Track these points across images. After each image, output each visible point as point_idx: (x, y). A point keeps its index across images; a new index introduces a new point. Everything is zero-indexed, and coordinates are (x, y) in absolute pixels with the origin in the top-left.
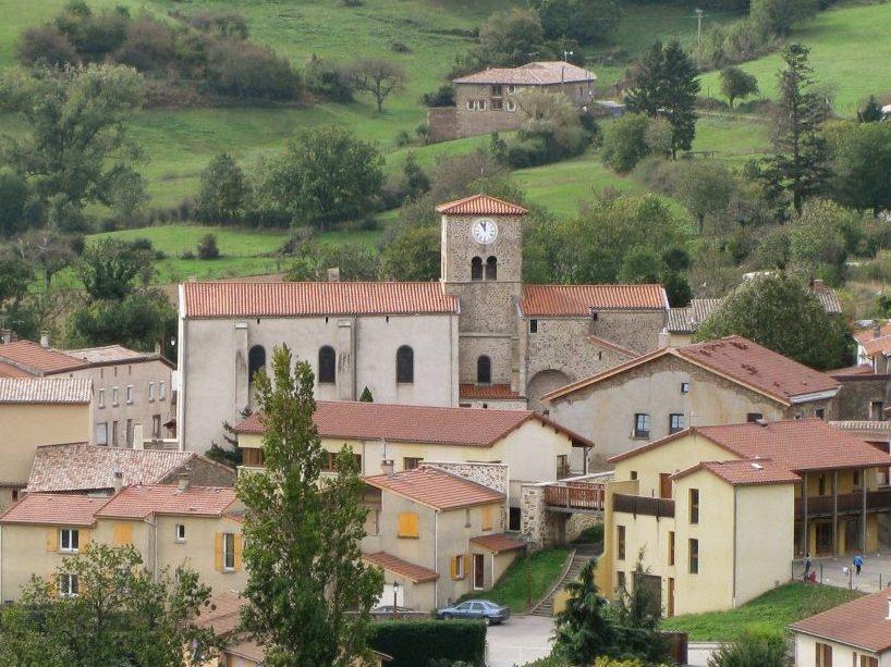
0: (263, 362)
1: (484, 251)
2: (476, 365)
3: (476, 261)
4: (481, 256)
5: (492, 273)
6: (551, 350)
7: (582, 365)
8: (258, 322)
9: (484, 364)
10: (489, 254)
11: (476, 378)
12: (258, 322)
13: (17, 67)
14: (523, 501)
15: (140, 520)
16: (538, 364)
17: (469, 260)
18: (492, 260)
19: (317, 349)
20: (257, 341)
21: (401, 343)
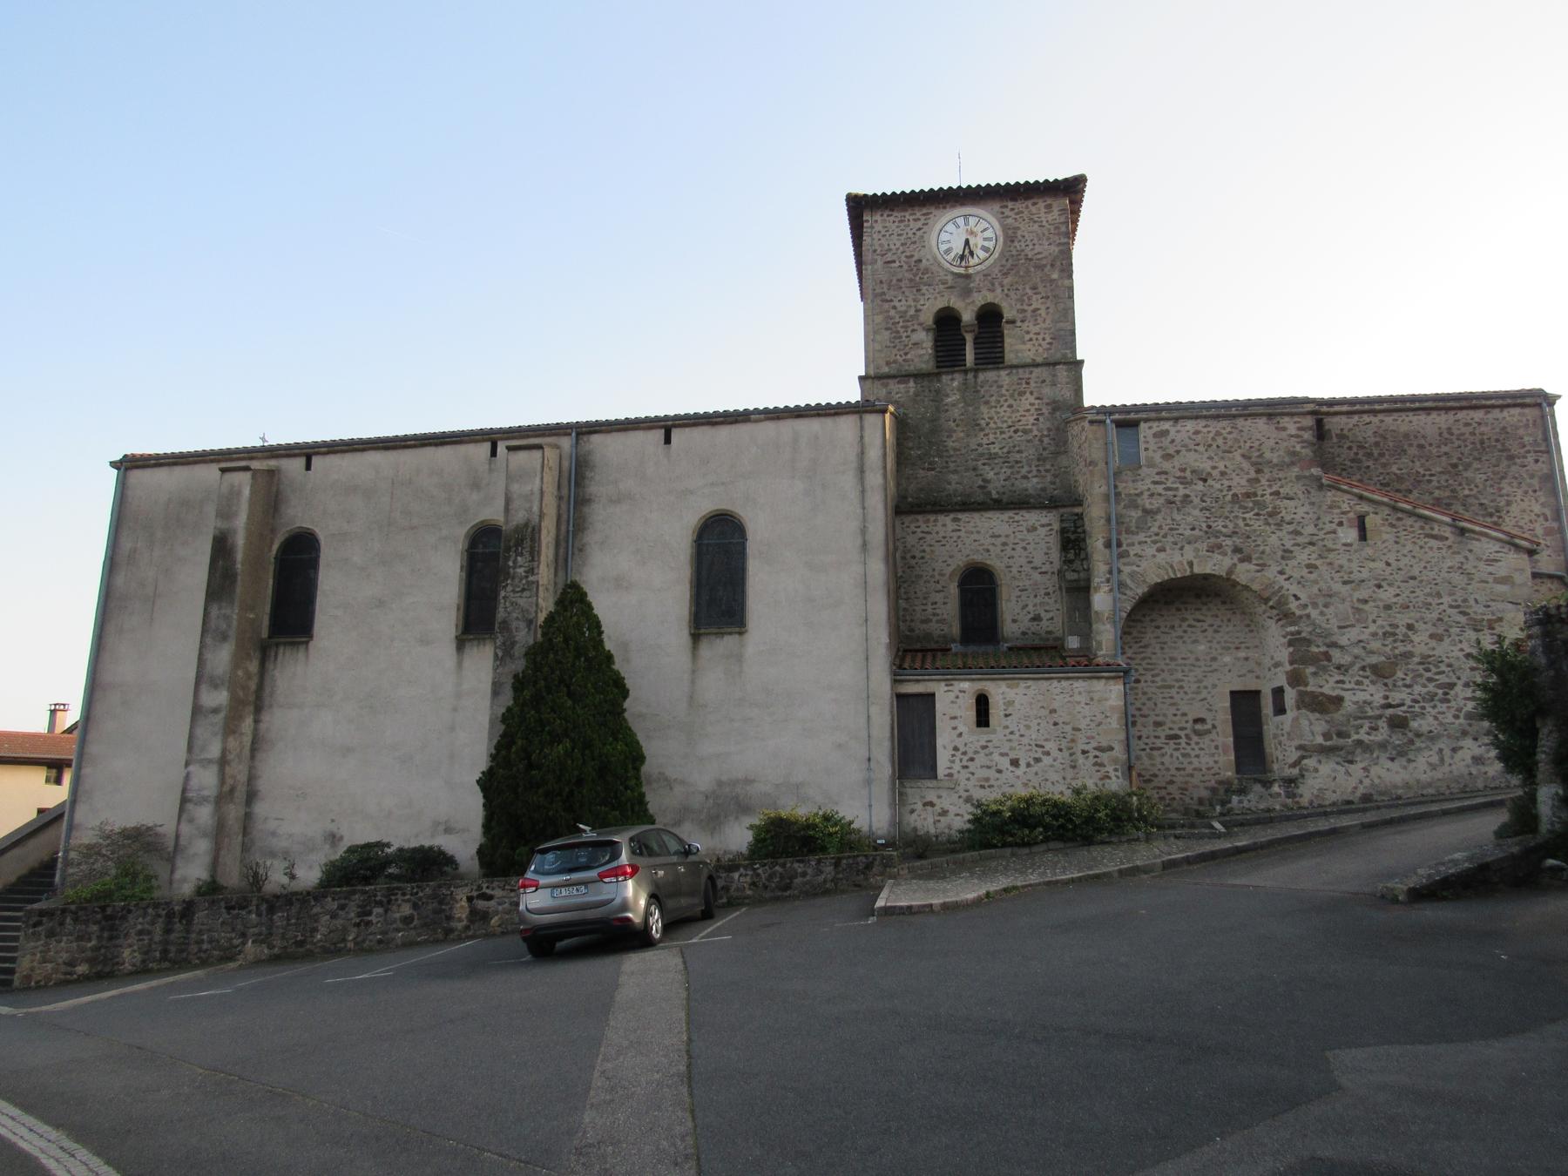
0: (234, 582)
1: (967, 292)
2: (954, 589)
3: (946, 322)
4: (956, 303)
5: (991, 354)
6: (1195, 514)
7: (1303, 556)
8: (668, 440)
9: (979, 586)
10: (980, 299)
11: (956, 629)
12: (668, 440)
13: (1493, 753)
14: (978, 794)
15: (187, 777)
16: (1154, 563)
17: (928, 317)
18: (990, 318)
19: (461, 532)
20: (297, 516)
21: (706, 506)
